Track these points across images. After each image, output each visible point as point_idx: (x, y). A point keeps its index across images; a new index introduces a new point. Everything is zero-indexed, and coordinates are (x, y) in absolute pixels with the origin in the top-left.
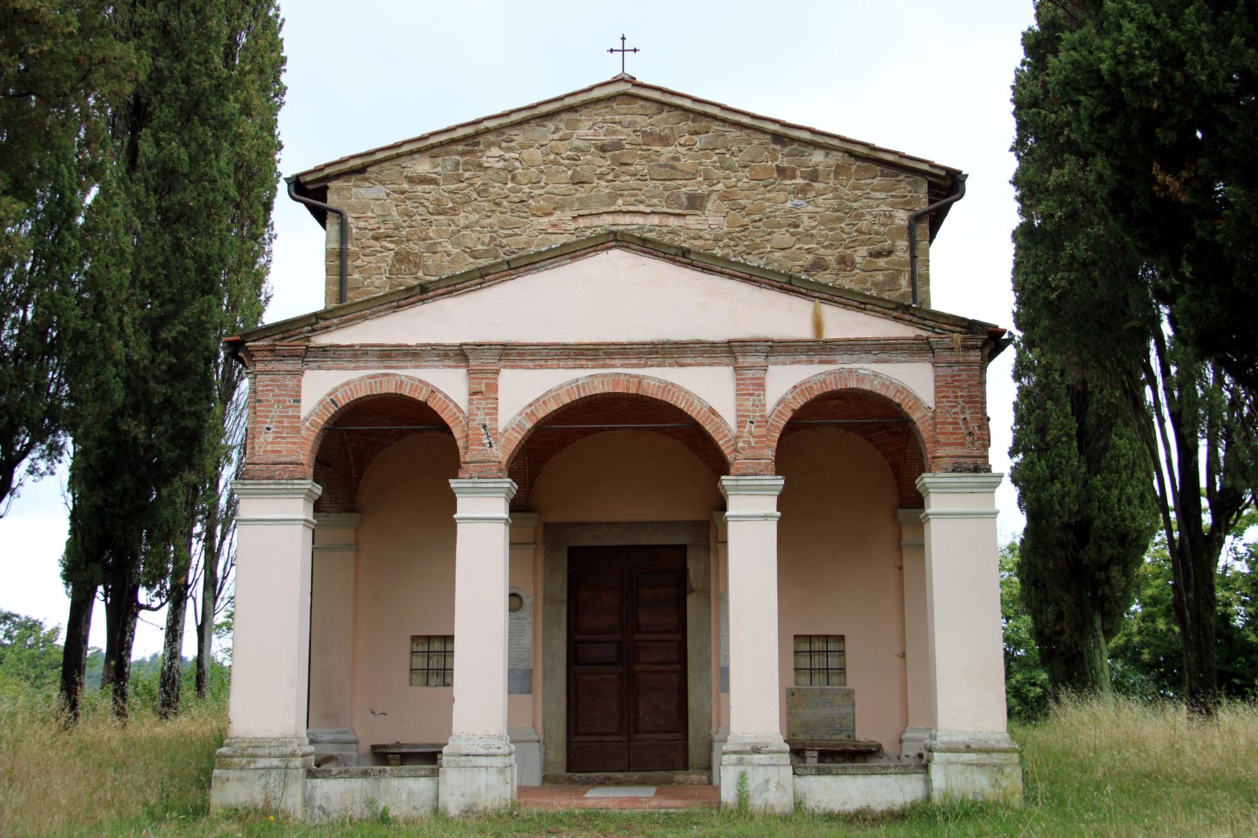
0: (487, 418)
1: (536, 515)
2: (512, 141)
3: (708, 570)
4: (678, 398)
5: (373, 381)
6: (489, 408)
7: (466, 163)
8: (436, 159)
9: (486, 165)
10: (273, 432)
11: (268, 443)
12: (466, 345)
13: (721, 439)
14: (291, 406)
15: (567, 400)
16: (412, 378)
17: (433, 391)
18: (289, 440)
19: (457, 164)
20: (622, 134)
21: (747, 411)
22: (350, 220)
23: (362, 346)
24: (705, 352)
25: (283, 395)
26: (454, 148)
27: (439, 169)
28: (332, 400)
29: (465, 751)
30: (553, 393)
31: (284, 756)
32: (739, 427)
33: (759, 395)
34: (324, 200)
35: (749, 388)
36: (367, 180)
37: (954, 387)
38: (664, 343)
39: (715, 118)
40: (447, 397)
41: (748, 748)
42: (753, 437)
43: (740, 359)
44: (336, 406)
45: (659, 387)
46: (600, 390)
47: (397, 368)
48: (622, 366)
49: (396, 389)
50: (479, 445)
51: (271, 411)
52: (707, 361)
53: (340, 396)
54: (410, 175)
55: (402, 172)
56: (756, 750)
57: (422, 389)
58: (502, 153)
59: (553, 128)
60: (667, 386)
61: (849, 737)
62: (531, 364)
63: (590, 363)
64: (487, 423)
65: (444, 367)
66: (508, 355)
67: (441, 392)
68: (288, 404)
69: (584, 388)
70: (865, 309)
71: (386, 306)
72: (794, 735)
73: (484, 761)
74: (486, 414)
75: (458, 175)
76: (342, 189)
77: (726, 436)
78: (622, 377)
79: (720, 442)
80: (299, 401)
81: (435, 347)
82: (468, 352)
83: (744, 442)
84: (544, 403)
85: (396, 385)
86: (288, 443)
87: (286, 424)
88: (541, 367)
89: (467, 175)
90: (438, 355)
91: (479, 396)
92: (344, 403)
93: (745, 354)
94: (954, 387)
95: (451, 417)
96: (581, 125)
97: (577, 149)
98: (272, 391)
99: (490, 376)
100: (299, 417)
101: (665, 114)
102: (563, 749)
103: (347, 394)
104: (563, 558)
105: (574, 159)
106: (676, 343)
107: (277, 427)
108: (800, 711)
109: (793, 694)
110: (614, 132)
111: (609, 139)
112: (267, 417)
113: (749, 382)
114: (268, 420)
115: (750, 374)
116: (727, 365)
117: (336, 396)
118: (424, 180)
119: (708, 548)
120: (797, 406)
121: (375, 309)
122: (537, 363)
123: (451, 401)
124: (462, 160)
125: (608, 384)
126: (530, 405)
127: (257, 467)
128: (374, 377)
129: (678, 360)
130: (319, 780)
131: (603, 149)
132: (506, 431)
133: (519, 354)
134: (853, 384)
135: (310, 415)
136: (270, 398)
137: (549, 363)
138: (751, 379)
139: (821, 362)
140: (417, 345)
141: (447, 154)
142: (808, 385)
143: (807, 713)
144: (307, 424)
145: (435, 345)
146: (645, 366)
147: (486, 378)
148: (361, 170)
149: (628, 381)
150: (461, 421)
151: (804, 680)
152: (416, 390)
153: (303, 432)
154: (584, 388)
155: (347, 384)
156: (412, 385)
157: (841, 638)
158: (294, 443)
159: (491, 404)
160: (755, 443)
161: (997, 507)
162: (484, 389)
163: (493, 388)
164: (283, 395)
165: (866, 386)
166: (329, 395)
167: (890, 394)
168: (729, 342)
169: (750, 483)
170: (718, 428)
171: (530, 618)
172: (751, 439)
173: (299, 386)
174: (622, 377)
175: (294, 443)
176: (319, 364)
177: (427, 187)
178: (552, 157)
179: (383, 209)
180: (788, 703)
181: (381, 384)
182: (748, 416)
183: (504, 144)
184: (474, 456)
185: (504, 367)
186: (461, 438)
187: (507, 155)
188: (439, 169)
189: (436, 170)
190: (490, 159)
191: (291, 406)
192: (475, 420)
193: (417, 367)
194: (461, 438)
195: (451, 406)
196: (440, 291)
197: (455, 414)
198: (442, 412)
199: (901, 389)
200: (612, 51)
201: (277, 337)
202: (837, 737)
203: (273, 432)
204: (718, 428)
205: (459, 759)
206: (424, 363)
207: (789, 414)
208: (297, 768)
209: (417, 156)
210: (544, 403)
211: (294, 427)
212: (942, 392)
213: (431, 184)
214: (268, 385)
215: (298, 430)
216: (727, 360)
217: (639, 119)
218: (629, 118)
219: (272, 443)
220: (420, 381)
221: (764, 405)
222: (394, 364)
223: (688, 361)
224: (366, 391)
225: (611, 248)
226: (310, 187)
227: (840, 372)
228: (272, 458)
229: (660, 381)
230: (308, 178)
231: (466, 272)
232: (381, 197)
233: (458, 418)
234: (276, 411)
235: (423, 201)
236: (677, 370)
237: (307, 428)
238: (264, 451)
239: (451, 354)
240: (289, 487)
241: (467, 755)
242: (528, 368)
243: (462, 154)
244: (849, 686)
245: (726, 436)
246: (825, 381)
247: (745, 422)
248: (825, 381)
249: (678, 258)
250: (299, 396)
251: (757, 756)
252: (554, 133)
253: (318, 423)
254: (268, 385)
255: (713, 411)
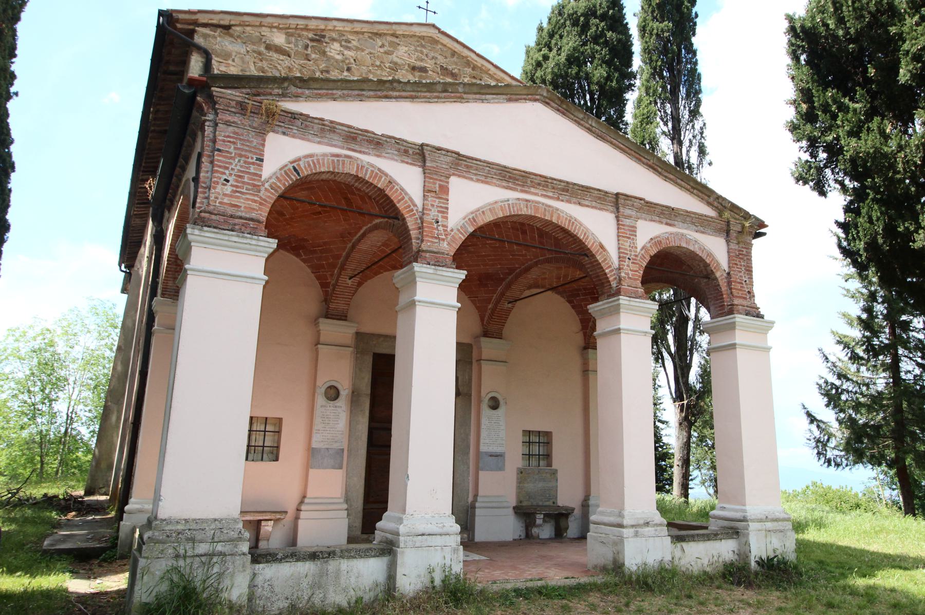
0: (440, 215)
1: (356, 325)
2: (350, 42)
3: (470, 379)
4: (579, 231)
5: (336, 159)
6: (441, 207)
7: (312, 46)
8: (290, 38)
9: (328, 53)
10: (232, 185)
11: (225, 195)
12: (427, 145)
13: (607, 268)
14: (253, 164)
15: (501, 215)
16: (372, 166)
17: (391, 182)
18: (248, 196)
19: (306, 47)
20: (427, 63)
21: (626, 249)
22: (213, 62)
23: (332, 122)
24: (600, 198)
25: (246, 151)
26: (305, 33)
27: (292, 46)
28: (294, 168)
29: (421, 531)
30: (492, 207)
31: (231, 540)
32: (620, 261)
33: (633, 239)
34: (192, 38)
35: (625, 233)
36: (231, 36)
37: (740, 258)
38: (575, 184)
39: (487, 72)
40: (402, 190)
41: (642, 522)
42: (631, 270)
43: (621, 209)
44: (298, 174)
45: (566, 219)
46: (525, 211)
47: (360, 152)
48: (542, 195)
49: (357, 171)
50: (432, 237)
51: (231, 164)
52: (598, 205)
53: (302, 166)
54: (268, 42)
55: (261, 39)
56: (647, 524)
57: (381, 177)
58: (342, 49)
59: (380, 44)
60: (572, 220)
61: (554, 503)
62: (474, 177)
63: (519, 188)
64: (440, 219)
65: (403, 162)
66: (457, 164)
67: (398, 184)
68: (250, 160)
69: (513, 207)
70: (692, 193)
71: (356, 92)
72: (521, 502)
73: (438, 540)
74: (439, 211)
75: (307, 55)
76: (209, 36)
77: (610, 267)
78: (541, 205)
79: (607, 271)
80: (262, 160)
81: (398, 141)
82: (427, 154)
83: (625, 273)
84: (483, 212)
85: (358, 168)
86: (248, 199)
87: (246, 180)
88: (483, 182)
89: (313, 56)
90: (399, 150)
91: (433, 194)
92: (306, 173)
93: (624, 206)
94: (740, 258)
95: (405, 208)
96: (399, 47)
97: (396, 64)
98: (234, 143)
99: (443, 178)
100: (260, 176)
101: (455, 59)
102: (360, 515)
103: (309, 165)
104: (369, 360)
105: (393, 70)
106: (583, 186)
107: (237, 181)
108: (526, 485)
109: (521, 473)
110: (422, 60)
111: (419, 64)
112: (227, 168)
113: (626, 228)
114: (227, 172)
115: (627, 222)
116: (612, 212)
117: (299, 165)
118: (279, 50)
119: (471, 363)
120: (652, 253)
121: (345, 92)
122: (479, 177)
123: (406, 194)
124: (311, 44)
125: (531, 208)
126: (472, 213)
127: (213, 217)
128: (338, 156)
129: (580, 201)
130: (261, 566)
131: (414, 68)
132: (452, 230)
133: (467, 166)
134: (684, 245)
135: (270, 178)
136: (232, 150)
137: (489, 180)
138: (628, 226)
139: (667, 224)
140: (383, 135)
141: (299, 36)
142: (659, 239)
143: (530, 486)
144: (267, 185)
145: (399, 139)
146: (558, 199)
147: (440, 180)
148: (227, 28)
149: (545, 209)
150: (414, 214)
151: (534, 462)
152: (375, 177)
153: (262, 193)
154: (513, 207)
155: (311, 156)
156: (372, 171)
157: (548, 434)
158: (255, 201)
159: (443, 203)
160: (632, 275)
161: (769, 344)
162: (437, 189)
163: (445, 190)
164: (246, 151)
165: (691, 248)
166: (292, 163)
167: (704, 256)
168: (617, 194)
169: (637, 304)
170: (605, 259)
171: (344, 408)
172: (630, 272)
173: (263, 145)
174: (541, 205)
175: (255, 201)
176: (284, 130)
177: (282, 57)
178: (378, 63)
179: (243, 62)
180: (518, 479)
181: (343, 164)
182: (627, 254)
183: (343, 43)
184: (429, 246)
185: (454, 174)
186: (414, 229)
187: (346, 52)
188: (292, 46)
189: (290, 46)
190: (332, 51)
191: (253, 164)
192: (428, 215)
193: (378, 156)
194: (414, 229)
195: (406, 198)
196: (404, 94)
197: (409, 206)
198: (399, 201)
199: (710, 254)
200: (420, 7)
201: (244, 90)
202: (547, 503)
203: (232, 185)
204: (605, 259)
205: (416, 539)
206: (384, 154)
207: (648, 258)
208: (244, 554)
209: (275, 30)
210: (483, 212)
211: (255, 185)
212: (733, 260)
213: (284, 55)
214: (228, 137)
215: (257, 188)
216: (611, 209)
217: (439, 57)
218: (432, 54)
219: (231, 196)
220: (379, 170)
221: (636, 248)
222: (357, 147)
223: (587, 203)
224: (328, 167)
225: (536, 100)
226: (179, 26)
227: (677, 234)
228: (230, 210)
229: (566, 214)
230: (181, 16)
231: (430, 83)
232: (242, 52)
233: (412, 210)
234: (236, 165)
235: (277, 65)
236: (578, 208)
237: (266, 189)
238: (219, 203)
239: (411, 152)
240: (254, 242)
241: (423, 535)
242: (471, 179)
243: (312, 40)
244: (554, 467)
245: (610, 267)
246: (668, 239)
247: (625, 257)
248: (668, 239)
249: (582, 122)
250: (263, 155)
251: (647, 529)
252: (381, 47)
253: (279, 187)
254: (228, 137)
255: (602, 246)
